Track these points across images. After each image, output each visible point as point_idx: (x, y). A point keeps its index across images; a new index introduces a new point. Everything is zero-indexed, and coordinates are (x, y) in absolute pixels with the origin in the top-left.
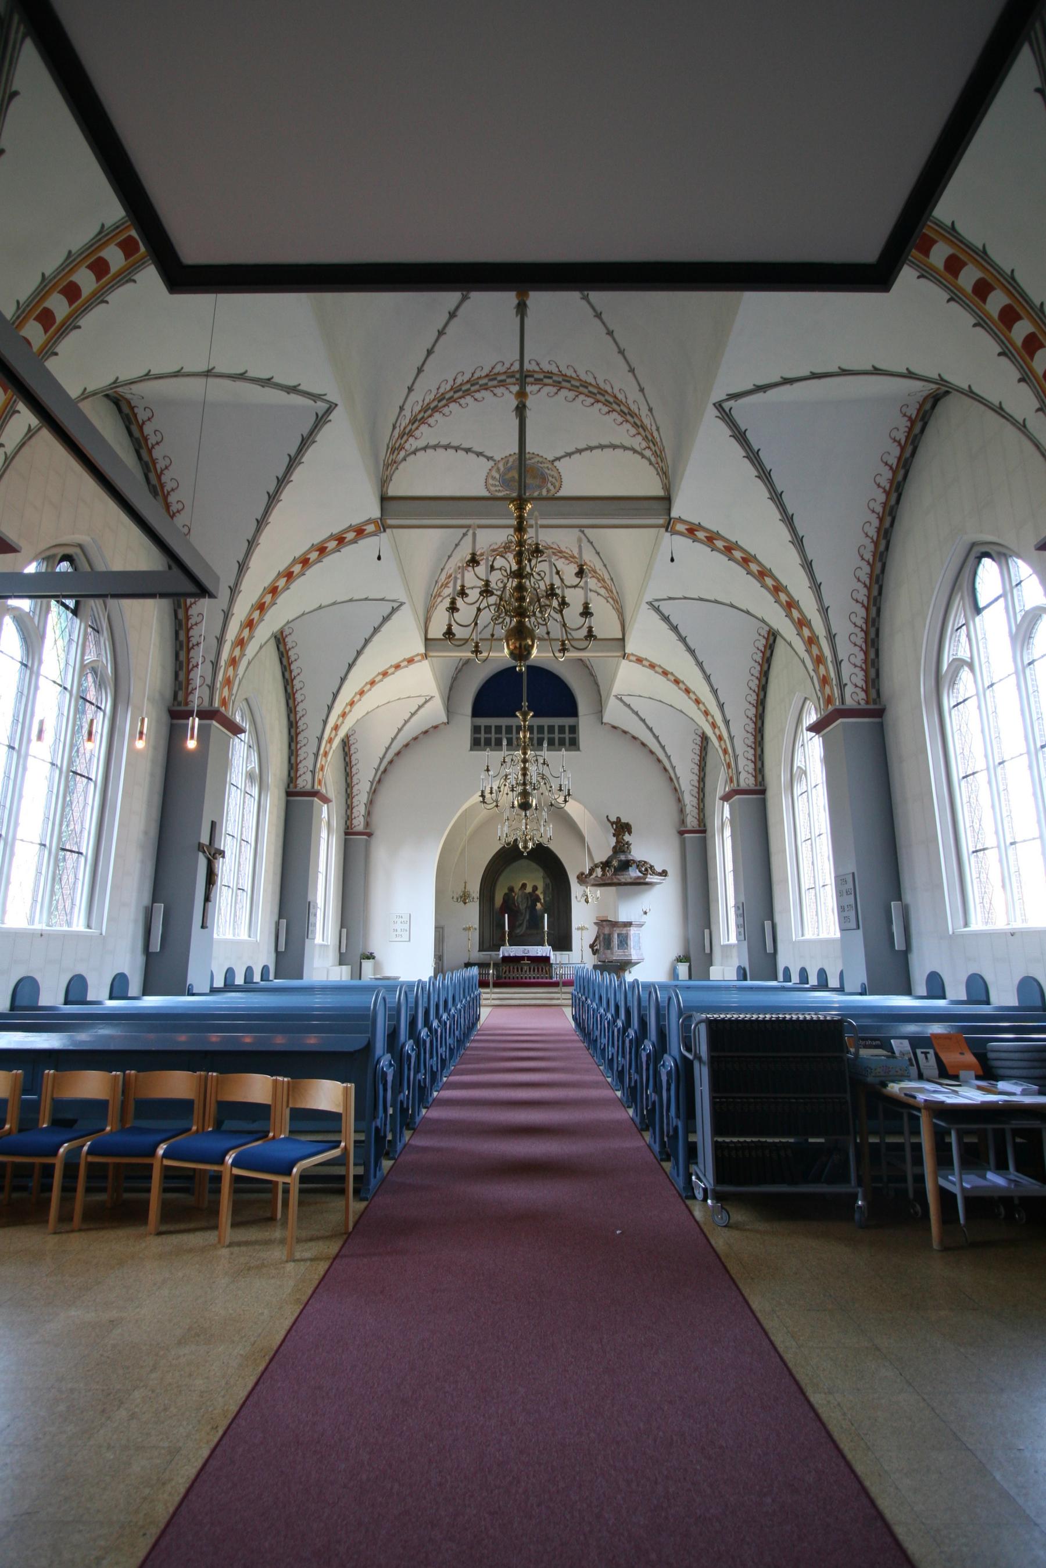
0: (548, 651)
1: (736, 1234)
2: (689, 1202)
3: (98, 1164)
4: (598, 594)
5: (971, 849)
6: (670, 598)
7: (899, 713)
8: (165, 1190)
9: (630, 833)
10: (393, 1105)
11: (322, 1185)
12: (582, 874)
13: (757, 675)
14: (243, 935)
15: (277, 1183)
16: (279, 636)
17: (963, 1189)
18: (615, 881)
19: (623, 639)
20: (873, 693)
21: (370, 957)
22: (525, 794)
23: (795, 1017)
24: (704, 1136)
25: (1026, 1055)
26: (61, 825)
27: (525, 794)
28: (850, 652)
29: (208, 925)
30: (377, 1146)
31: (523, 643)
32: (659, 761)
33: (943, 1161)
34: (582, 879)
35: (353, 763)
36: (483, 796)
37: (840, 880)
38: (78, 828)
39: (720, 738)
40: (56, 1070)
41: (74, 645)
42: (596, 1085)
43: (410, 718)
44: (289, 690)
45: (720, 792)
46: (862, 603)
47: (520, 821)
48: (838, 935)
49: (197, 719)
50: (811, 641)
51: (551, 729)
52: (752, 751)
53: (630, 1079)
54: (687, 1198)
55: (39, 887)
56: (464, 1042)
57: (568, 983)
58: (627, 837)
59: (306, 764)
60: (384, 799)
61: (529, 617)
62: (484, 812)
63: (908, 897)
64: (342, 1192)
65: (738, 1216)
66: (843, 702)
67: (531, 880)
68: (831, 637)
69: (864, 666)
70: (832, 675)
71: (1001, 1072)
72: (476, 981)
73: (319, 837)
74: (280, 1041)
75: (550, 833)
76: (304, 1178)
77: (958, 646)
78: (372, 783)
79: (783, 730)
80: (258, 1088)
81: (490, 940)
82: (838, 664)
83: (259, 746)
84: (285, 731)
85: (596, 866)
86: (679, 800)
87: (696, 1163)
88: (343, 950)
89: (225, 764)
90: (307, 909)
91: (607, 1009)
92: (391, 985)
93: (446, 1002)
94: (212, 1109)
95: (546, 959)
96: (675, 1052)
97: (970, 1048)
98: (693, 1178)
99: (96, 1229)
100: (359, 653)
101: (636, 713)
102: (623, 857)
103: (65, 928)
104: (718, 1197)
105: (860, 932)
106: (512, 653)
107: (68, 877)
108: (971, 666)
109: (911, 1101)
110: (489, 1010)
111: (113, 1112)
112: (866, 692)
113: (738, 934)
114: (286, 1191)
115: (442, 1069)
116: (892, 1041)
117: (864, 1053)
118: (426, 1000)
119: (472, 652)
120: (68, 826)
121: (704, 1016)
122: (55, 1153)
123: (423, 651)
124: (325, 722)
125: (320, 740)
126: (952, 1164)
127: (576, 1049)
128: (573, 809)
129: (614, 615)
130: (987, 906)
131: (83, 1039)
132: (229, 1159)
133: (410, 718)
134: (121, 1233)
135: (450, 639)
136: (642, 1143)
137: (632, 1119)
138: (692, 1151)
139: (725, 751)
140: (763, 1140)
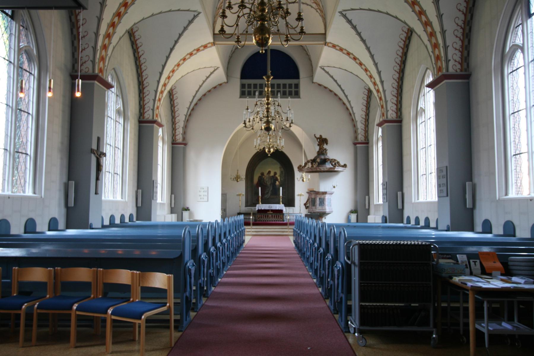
0: (278, 41)
1: (369, 350)
2: (346, 334)
3: (45, 313)
4: (312, 7)
5: (513, 154)
6: (352, 9)
7: (479, 76)
8: (78, 326)
9: (327, 144)
10: (196, 285)
11: (157, 324)
12: (300, 166)
13: (401, 54)
14: (119, 198)
15: (135, 323)
16: (131, 32)
17: (488, 330)
18: (318, 170)
19: (325, 34)
20: (465, 65)
21: (187, 209)
22: (268, 122)
23: (413, 243)
24: (355, 302)
25: (529, 264)
26: (15, 139)
27: (268, 122)
28: (453, 41)
29: (99, 192)
30: (186, 305)
31: (264, 36)
32: (344, 104)
33: (479, 316)
34: (300, 169)
35: (175, 105)
36: (245, 123)
37: (439, 170)
38: (24, 141)
39: (378, 91)
40: (19, 267)
41: (13, 37)
42: (304, 276)
43: (206, 79)
44: (138, 64)
45: (377, 121)
46: (463, 12)
47: (267, 137)
48: (437, 200)
49: (80, 81)
50: (432, 35)
51: (284, 86)
52: (395, 99)
53: (320, 273)
54: (346, 332)
55: (5, 172)
56: (235, 254)
57: (292, 224)
58: (325, 146)
59: (149, 106)
60: (194, 125)
61: (267, 21)
62: (247, 133)
63: (476, 180)
64: (168, 327)
65: (371, 341)
66: (447, 70)
67: (274, 169)
68: (443, 32)
69: (461, 49)
70: (442, 54)
71: (515, 272)
72: (243, 222)
73: (157, 145)
74: (137, 253)
75: (283, 144)
76: (148, 321)
77: (516, 37)
78: (186, 116)
79: (413, 87)
80: (124, 276)
81: (251, 201)
82: (446, 48)
83: (122, 94)
84: (137, 87)
85: (308, 162)
86: (354, 126)
87: (351, 315)
88: (173, 206)
89: (103, 106)
90: (152, 184)
91: (310, 238)
92: (194, 224)
93: (225, 233)
94: (101, 287)
95: (281, 211)
96: (342, 260)
97: (499, 260)
98: (349, 322)
99: (44, 345)
100: (176, 42)
101: (332, 77)
102: (323, 157)
103: (22, 194)
104: (361, 332)
105: (448, 198)
106: (257, 42)
107: (21, 167)
108: (522, 49)
109: (464, 286)
110: (250, 237)
111: (50, 288)
112: (461, 64)
113: (383, 198)
114: (139, 327)
115: (223, 267)
116: (458, 256)
117: (442, 261)
118: (213, 232)
119: (236, 42)
120: (19, 139)
121: (357, 242)
122: (20, 308)
123: (212, 41)
124: (159, 82)
125: (156, 92)
126: (483, 318)
127: (294, 258)
128: (295, 129)
129: (320, 19)
130: (519, 184)
131: (35, 251)
132: (110, 312)
133: (206, 79)
134: (57, 347)
135: (222, 34)
136: (325, 305)
137: (321, 293)
138: (349, 310)
139: (381, 99)
140: (386, 304)
